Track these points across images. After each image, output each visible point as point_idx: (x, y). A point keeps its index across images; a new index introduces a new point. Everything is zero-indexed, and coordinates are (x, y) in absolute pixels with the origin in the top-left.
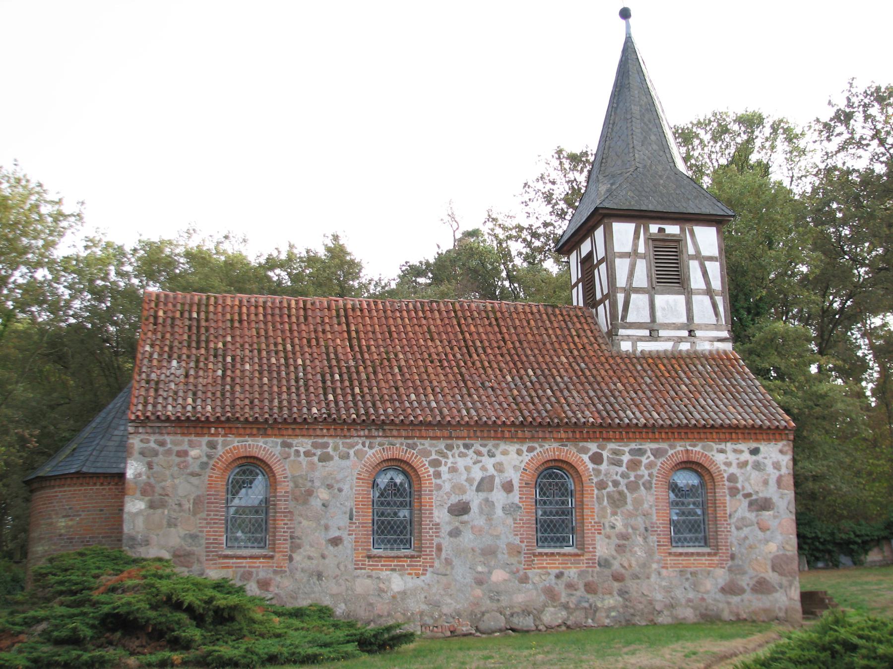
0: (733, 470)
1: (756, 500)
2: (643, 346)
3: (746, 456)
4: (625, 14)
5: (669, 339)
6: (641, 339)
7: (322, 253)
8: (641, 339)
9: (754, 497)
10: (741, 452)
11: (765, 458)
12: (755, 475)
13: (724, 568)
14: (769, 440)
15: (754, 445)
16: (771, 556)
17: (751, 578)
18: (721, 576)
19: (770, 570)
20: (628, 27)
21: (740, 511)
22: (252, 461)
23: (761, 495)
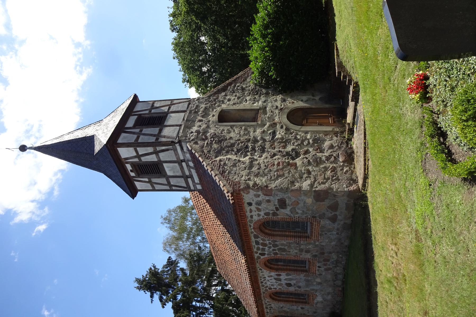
0: (262, 213)
1: (279, 205)
2: (197, 180)
3: (253, 207)
4: (23, 148)
5: (190, 171)
6: (193, 181)
7: (175, 34)
8: (193, 181)
9: (278, 206)
10: (251, 209)
11: (253, 200)
12: (264, 205)
13: (320, 221)
14: (242, 199)
15: (246, 205)
16: (314, 201)
17: (327, 211)
18: (325, 222)
19: (324, 203)
20: (31, 148)
21: (286, 212)
22: (269, 265)
23: (276, 204)
